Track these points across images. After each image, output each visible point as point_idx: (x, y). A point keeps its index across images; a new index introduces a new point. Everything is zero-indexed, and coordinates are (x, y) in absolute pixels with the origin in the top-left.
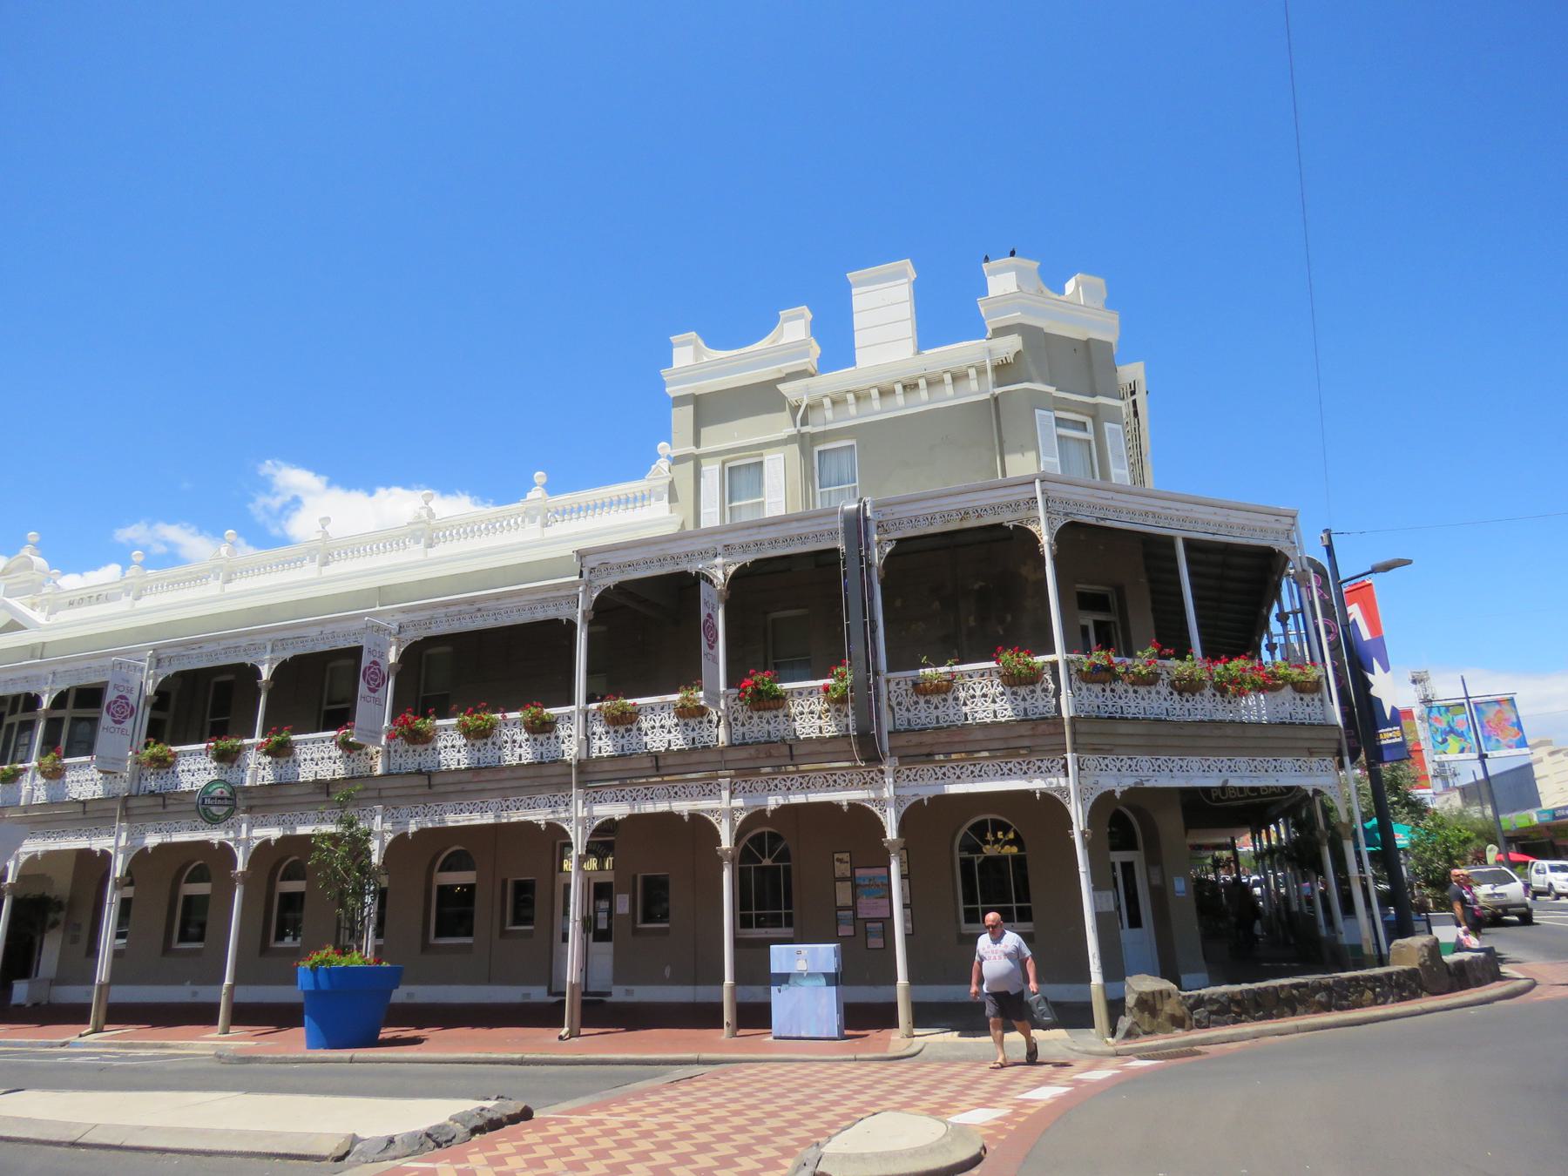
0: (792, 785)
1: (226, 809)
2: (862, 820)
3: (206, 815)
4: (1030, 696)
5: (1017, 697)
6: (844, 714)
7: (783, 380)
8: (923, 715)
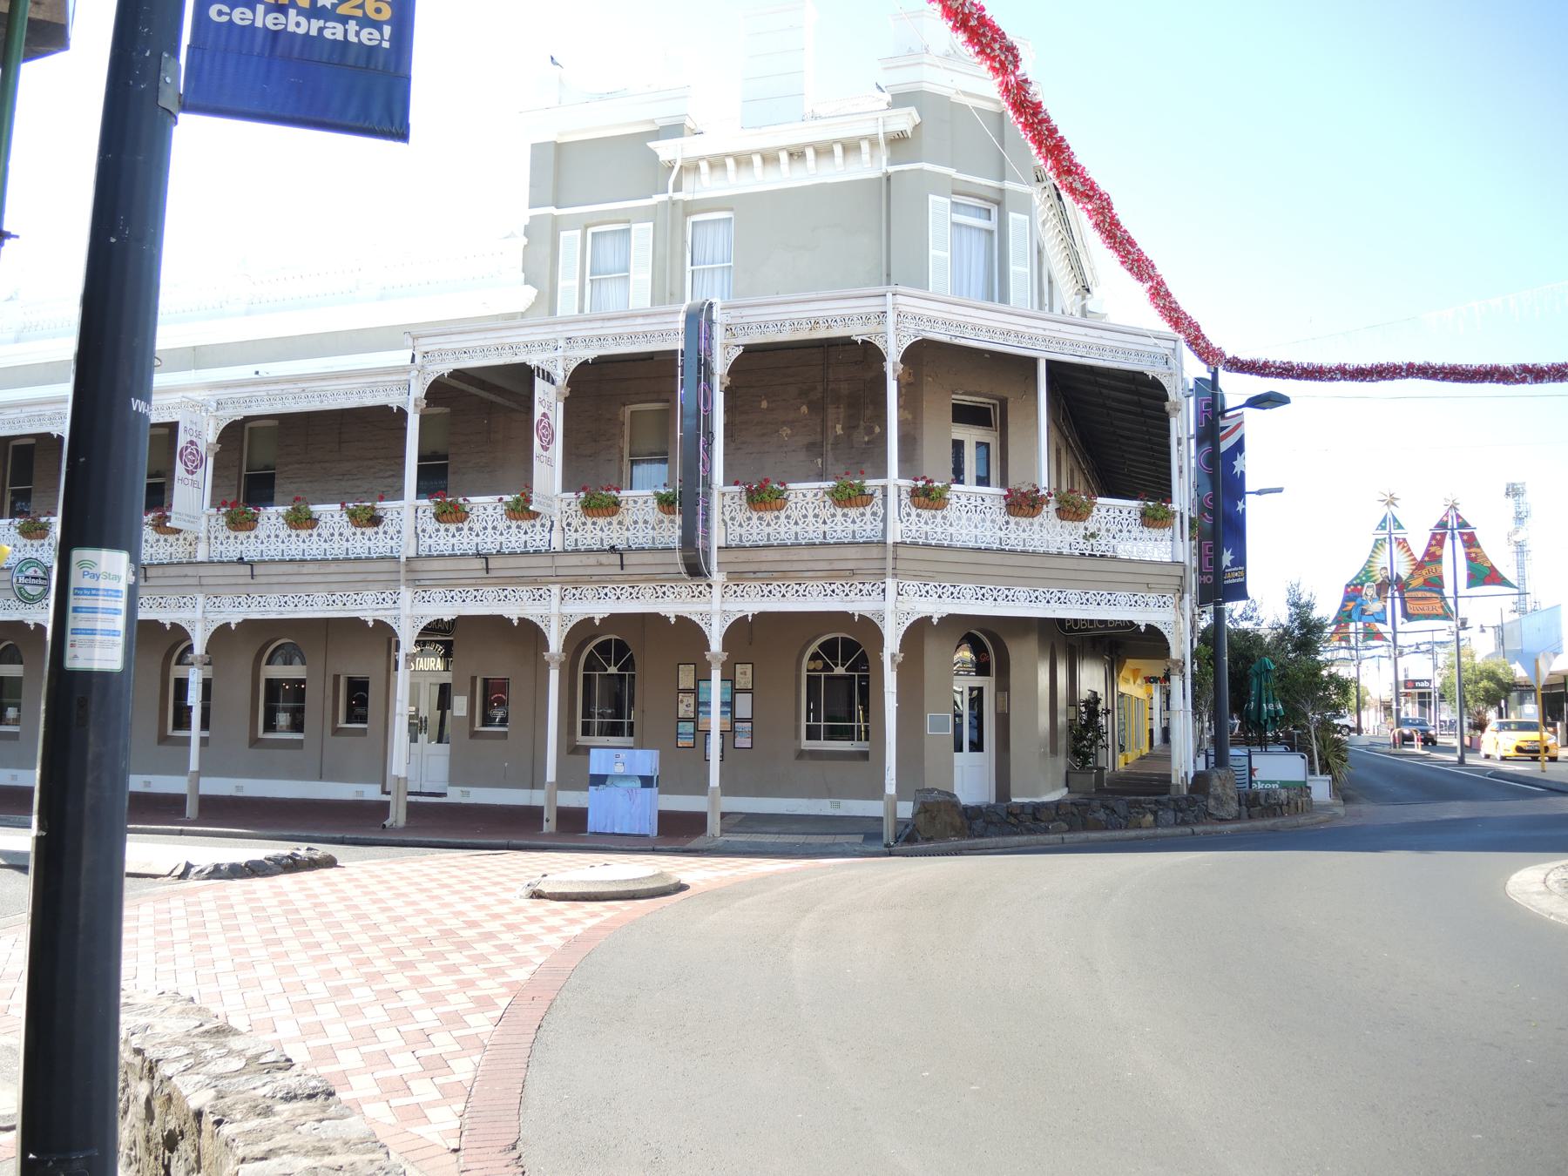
0: (621, 594)
1: (41, 588)
2: (688, 633)
3: (22, 595)
4: (860, 519)
5: (763, 523)
6: (625, 527)
7: (658, 135)
8: (754, 531)
